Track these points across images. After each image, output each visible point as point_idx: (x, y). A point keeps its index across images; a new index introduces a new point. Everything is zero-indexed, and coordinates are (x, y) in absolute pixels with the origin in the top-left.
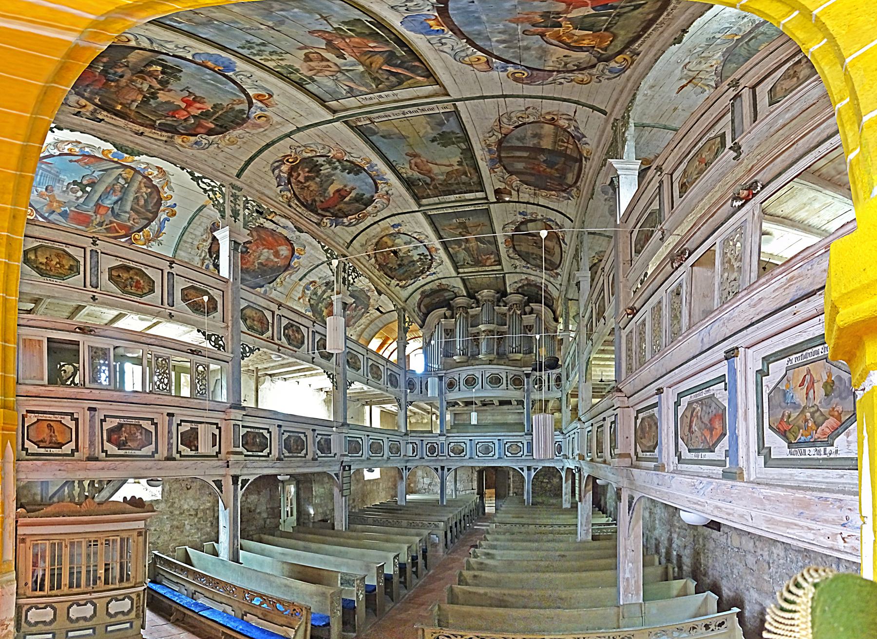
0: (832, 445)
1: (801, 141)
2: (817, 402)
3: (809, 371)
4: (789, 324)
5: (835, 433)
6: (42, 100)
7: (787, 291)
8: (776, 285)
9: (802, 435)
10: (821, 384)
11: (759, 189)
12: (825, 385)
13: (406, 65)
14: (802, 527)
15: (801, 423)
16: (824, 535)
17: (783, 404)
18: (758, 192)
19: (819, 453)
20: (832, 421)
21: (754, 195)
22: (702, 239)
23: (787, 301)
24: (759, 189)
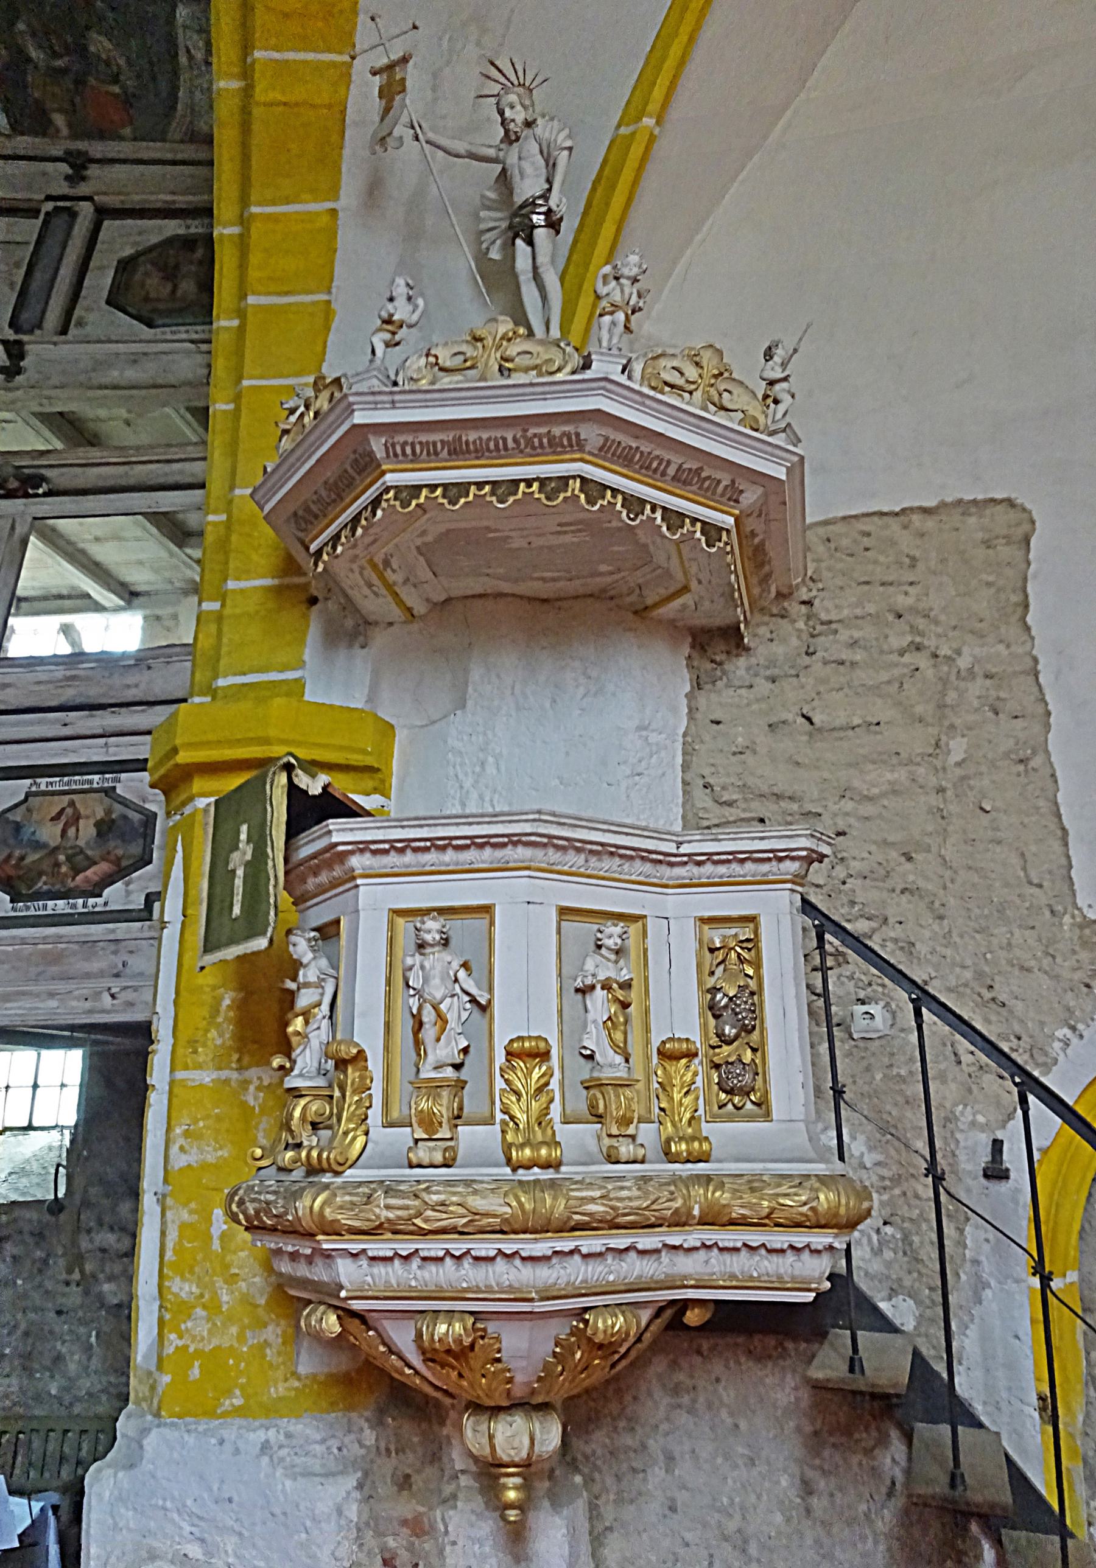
0: (100, 896)
1: (140, 467)
2: (81, 843)
3: (72, 804)
4: (50, 735)
5: (109, 880)
6: (790, 798)
7: (60, 691)
8: (43, 677)
9: (45, 883)
10: (92, 821)
11: (40, 491)
12: (98, 824)
13: (45, 851)
14: (38, 995)
15: (46, 866)
16: (78, 999)
17: (11, 841)
18: (37, 495)
19: (74, 906)
20: (104, 867)
21: (27, 496)
22: (89, 733)
23: (54, 703)
24: (40, 491)
